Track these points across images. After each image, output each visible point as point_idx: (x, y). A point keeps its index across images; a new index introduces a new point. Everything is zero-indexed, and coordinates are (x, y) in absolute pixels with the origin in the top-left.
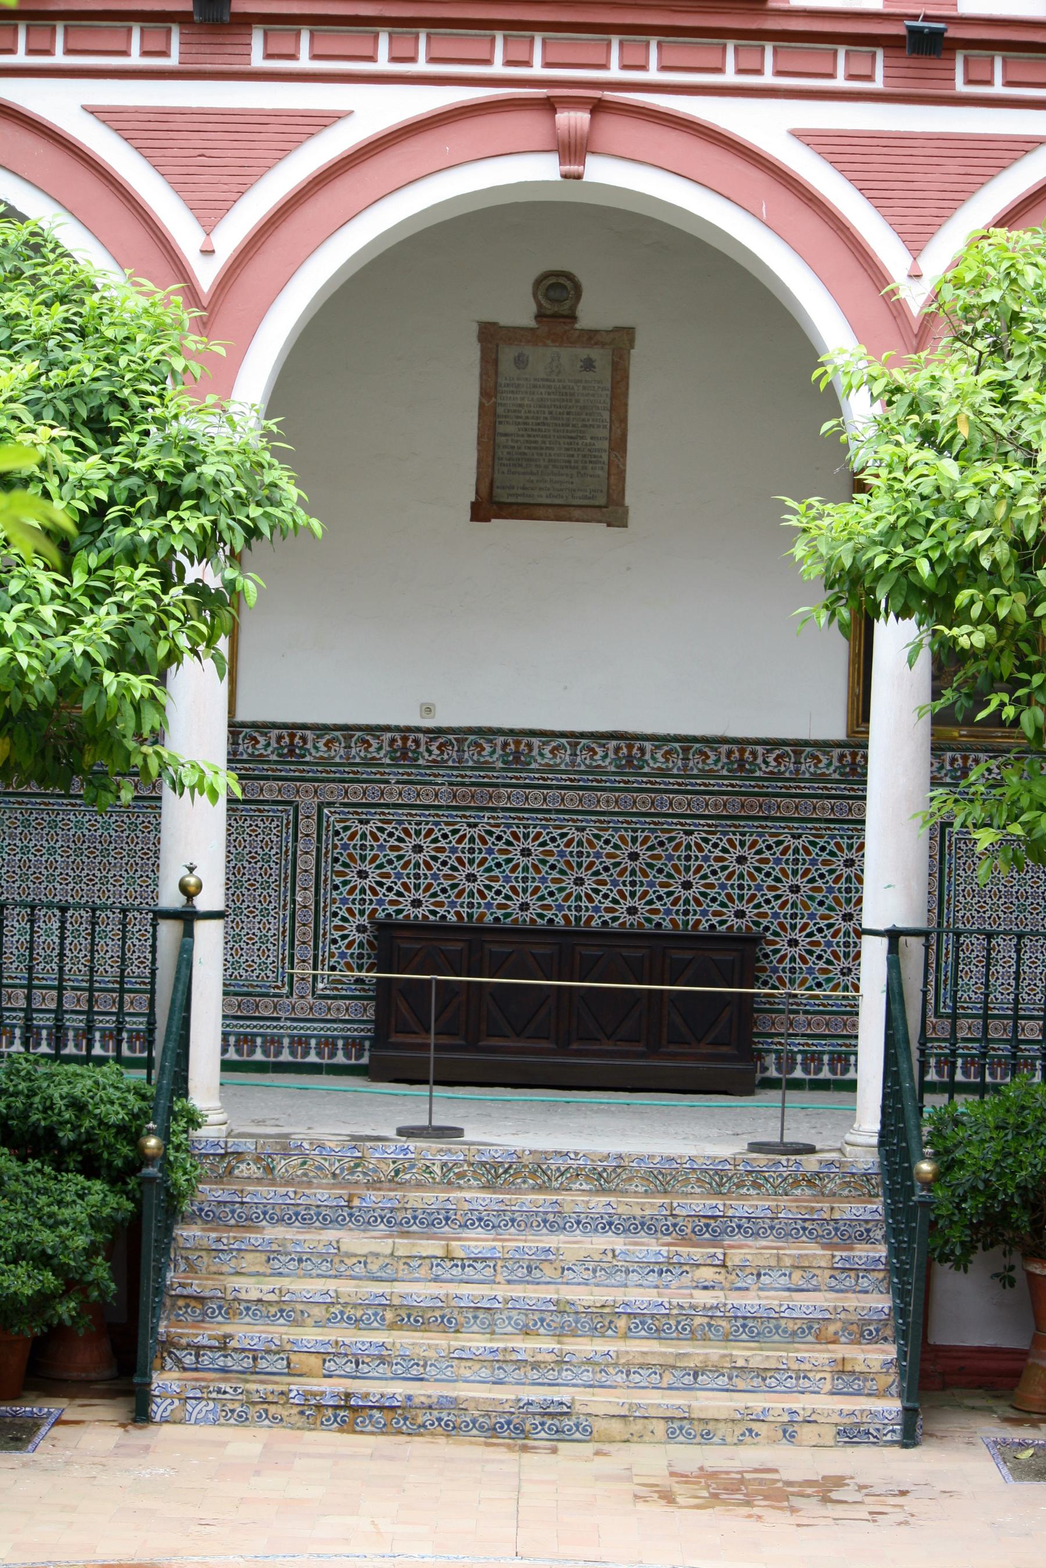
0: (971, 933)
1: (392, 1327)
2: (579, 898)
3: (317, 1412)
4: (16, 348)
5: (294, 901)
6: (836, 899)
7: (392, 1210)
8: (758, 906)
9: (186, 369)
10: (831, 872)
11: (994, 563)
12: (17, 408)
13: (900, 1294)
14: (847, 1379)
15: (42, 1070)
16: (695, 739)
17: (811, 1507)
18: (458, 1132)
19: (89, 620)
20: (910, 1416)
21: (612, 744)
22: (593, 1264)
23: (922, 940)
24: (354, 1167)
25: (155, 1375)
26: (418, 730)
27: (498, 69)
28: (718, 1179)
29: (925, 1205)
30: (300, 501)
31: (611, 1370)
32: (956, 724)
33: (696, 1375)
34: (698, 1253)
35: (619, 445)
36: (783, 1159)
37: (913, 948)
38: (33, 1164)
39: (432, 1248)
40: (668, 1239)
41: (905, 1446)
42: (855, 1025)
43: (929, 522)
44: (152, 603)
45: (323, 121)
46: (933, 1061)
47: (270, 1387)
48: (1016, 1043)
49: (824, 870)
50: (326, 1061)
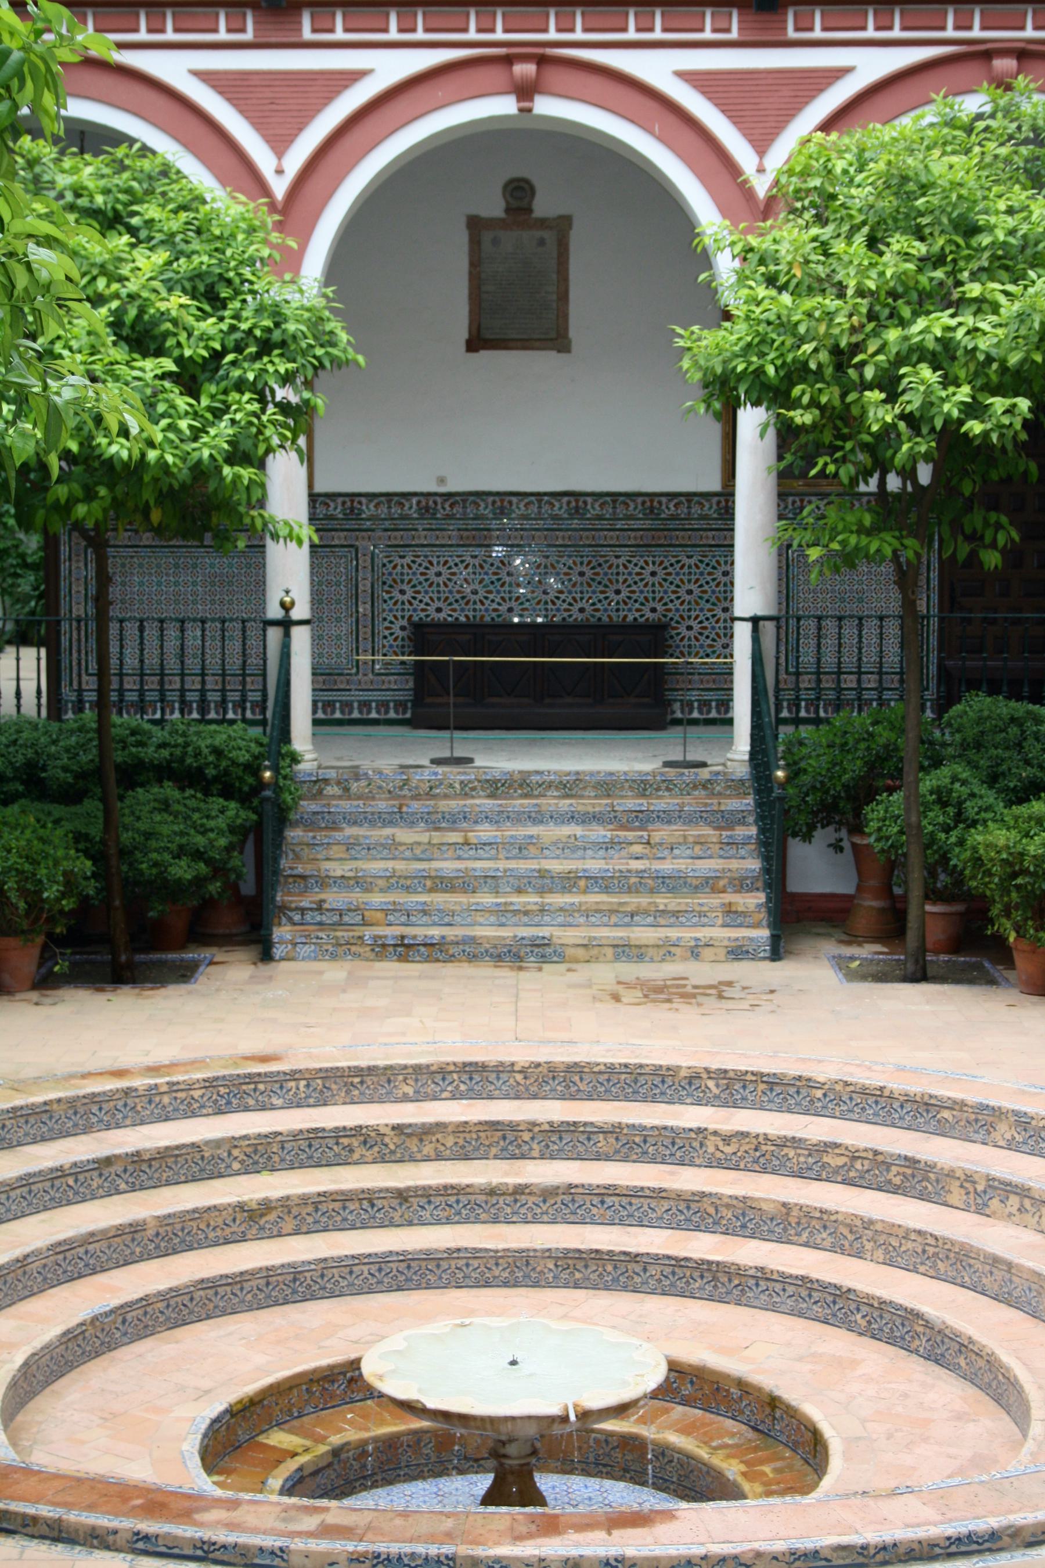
0: (809, 617)
1: (431, 890)
2: (546, 603)
3: (382, 949)
4: (153, 243)
5: (357, 612)
6: (717, 598)
7: (428, 813)
8: (665, 604)
9: (270, 256)
10: (714, 580)
11: (820, 365)
12: (155, 284)
13: (766, 858)
14: (732, 915)
15: (193, 729)
16: (620, 494)
17: (711, 1002)
18: (470, 760)
19: (212, 431)
20: (775, 940)
21: (565, 499)
22: (562, 843)
23: (774, 623)
25: (275, 929)
26: (436, 494)
27: (472, 35)
28: (643, 786)
29: (781, 799)
30: (349, 342)
31: (576, 915)
32: (794, 477)
33: (632, 916)
34: (631, 835)
35: (564, 297)
36: (686, 771)
37: (769, 629)
38: (189, 792)
39: (455, 837)
40: (611, 827)
41: (773, 960)
42: (732, 682)
43: (773, 341)
44: (255, 421)
45: (354, 77)
46: (785, 704)
47: (351, 934)
48: (839, 690)
49: (709, 578)
50: (382, 717)
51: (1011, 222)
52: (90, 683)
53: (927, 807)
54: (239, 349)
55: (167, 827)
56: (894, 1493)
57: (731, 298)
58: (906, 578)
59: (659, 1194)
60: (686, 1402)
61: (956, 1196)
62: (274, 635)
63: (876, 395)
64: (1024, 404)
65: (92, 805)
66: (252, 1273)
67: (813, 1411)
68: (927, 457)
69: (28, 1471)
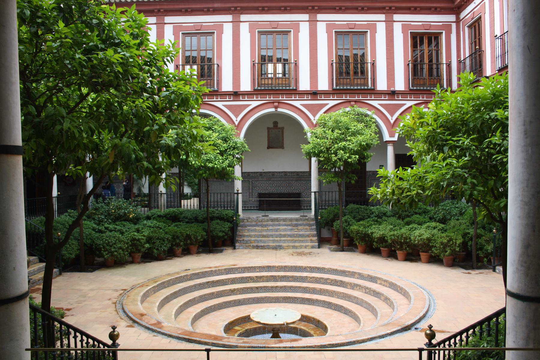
13: (317, 231)
14: (312, 241)
17: (308, 255)
20: (319, 245)
22: (284, 229)
24: (257, 220)
27: (268, 99)
28: (297, 220)
35: (283, 140)
39: (266, 228)
45: (404, 104)
51: (354, 128)
52: (206, 203)
53: (344, 223)
54: (230, 149)
55: (218, 227)
56: (338, 335)
57: (310, 140)
58: (339, 185)
59: (300, 287)
60: (304, 321)
61: (349, 287)
62: (236, 195)
63: (334, 155)
64: (357, 156)
65: (206, 224)
66: (232, 301)
67: (325, 322)
68: (342, 165)
69: (195, 333)
